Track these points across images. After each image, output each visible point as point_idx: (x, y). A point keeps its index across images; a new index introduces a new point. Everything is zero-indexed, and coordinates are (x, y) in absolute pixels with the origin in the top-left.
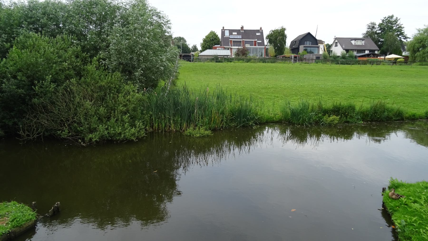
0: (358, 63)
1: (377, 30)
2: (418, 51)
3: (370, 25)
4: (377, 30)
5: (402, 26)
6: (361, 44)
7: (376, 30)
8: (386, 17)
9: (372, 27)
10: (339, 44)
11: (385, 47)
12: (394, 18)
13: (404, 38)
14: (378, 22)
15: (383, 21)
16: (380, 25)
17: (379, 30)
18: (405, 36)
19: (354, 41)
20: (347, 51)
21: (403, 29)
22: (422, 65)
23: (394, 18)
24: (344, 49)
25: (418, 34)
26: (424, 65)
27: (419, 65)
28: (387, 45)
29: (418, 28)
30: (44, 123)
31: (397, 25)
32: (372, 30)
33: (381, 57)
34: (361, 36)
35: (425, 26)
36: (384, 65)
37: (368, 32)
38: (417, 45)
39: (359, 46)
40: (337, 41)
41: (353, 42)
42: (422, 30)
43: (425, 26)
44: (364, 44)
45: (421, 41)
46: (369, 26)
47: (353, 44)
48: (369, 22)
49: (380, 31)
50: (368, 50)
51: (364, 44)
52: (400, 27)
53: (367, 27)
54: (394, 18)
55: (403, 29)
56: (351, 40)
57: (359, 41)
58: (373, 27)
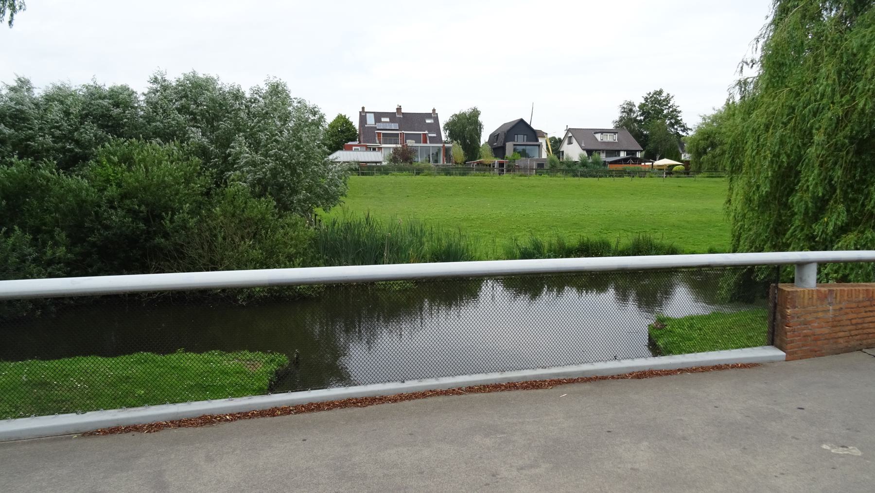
0: (610, 174)
2: (705, 153)
3: (625, 106)
5: (678, 109)
6: (612, 140)
8: (650, 93)
9: (628, 109)
10: (574, 141)
11: (651, 146)
12: (664, 94)
13: (681, 130)
14: (638, 101)
15: (646, 99)
20: (590, 152)
25: (703, 124)
29: (702, 115)
31: (670, 107)
34: (611, 126)
35: (714, 109)
37: (622, 119)
38: (703, 143)
39: (609, 143)
40: (570, 135)
41: (598, 136)
43: (714, 109)
44: (616, 141)
45: (709, 137)
46: (624, 108)
50: (625, 151)
51: (616, 141)
54: (663, 95)
56: (595, 133)
57: (608, 134)
58: (631, 110)
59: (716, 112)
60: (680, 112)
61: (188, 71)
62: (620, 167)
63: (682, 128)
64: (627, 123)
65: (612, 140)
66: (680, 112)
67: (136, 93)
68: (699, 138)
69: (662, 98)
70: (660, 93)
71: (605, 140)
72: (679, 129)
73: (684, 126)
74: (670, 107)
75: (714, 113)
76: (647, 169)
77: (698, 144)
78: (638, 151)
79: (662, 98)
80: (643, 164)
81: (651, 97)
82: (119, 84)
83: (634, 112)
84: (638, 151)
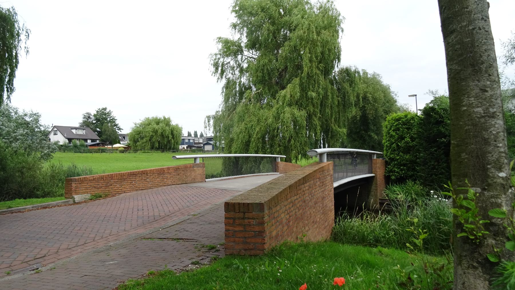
0: (90, 152)
1: (93, 119)
2: (138, 141)
3: (86, 115)
4: (93, 119)
5: (116, 118)
6: (82, 133)
7: (91, 120)
8: (100, 109)
9: (87, 117)
10: (58, 133)
11: (104, 137)
12: (108, 110)
13: (118, 129)
14: (93, 112)
15: (97, 112)
16: (95, 115)
17: (94, 120)
18: (118, 127)
19: (75, 130)
20: (70, 140)
21: (116, 121)
22: (145, 153)
23: (108, 110)
24: (66, 138)
25: (135, 127)
26: (146, 153)
27: (143, 153)
28: (107, 135)
29: (134, 122)
30: (386, 195)
31: (111, 117)
32: (88, 120)
33: (108, 146)
34: (77, 125)
35: (140, 120)
36: (129, 153)
37: (84, 122)
38: (137, 136)
39: (80, 135)
40: (55, 129)
41: (74, 131)
42: (138, 124)
43: (140, 120)
44: (85, 134)
45: (140, 133)
46: (85, 116)
47: (75, 133)
48: (84, 112)
49: (95, 122)
50: (90, 139)
51: (85, 134)
52: (114, 119)
53: (83, 116)
54: (107, 110)
55: (116, 121)
56: (71, 129)
57: (80, 130)
58: (89, 117)
59: (141, 122)
60: (116, 120)
61: (16, 77)
62: (96, 148)
63: (118, 129)
64: (86, 124)
65: (82, 134)
66: (116, 120)
67: (59, 142)
68: (134, 134)
69: (107, 112)
70: (105, 109)
71: (78, 133)
72: (116, 128)
73: (119, 128)
74: (111, 117)
75: (141, 122)
76: (109, 148)
77: (134, 137)
78: (98, 140)
79: (107, 112)
80: (106, 146)
81: (100, 111)
82: (139, 121)
83: (91, 118)
84: (98, 140)
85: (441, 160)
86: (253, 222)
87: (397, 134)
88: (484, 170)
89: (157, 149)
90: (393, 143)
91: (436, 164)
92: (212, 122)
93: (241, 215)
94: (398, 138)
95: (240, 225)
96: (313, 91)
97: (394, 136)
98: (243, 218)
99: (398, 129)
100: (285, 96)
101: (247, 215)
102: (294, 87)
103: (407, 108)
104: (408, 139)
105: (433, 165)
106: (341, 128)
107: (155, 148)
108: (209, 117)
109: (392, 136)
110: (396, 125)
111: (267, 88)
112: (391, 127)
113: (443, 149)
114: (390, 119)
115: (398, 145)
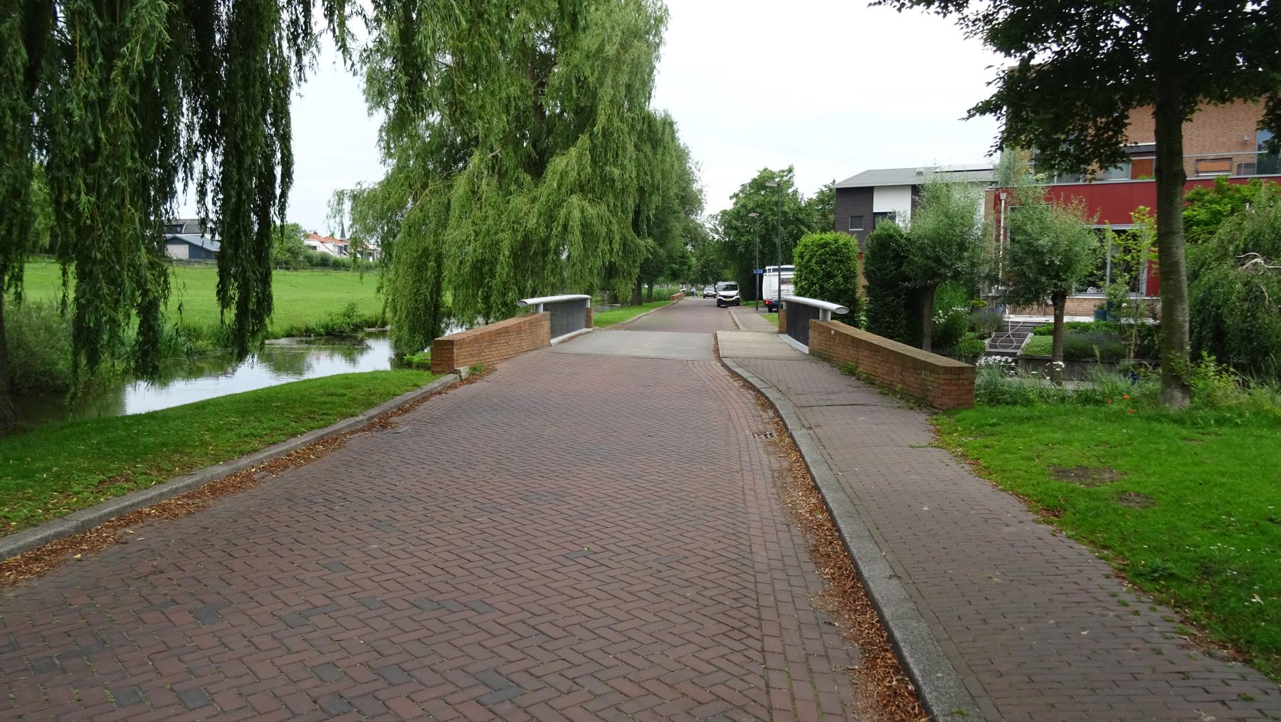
85: (900, 315)
86: (966, 382)
87: (822, 269)
88: (1182, 346)
89: (47, 252)
90: (816, 283)
91: (892, 320)
92: (347, 205)
93: (956, 377)
94: (823, 276)
95: (954, 385)
96: (615, 166)
97: (816, 272)
98: (958, 379)
99: (824, 262)
100: (564, 175)
101: (961, 377)
102: (580, 156)
103: (260, 39)
104: (840, 279)
105: (887, 322)
106: (644, 238)
107: (41, 250)
108: (340, 195)
109: (812, 271)
110: (821, 255)
111: (510, 147)
112: (812, 257)
113: (902, 300)
114: (810, 244)
115: (822, 287)
